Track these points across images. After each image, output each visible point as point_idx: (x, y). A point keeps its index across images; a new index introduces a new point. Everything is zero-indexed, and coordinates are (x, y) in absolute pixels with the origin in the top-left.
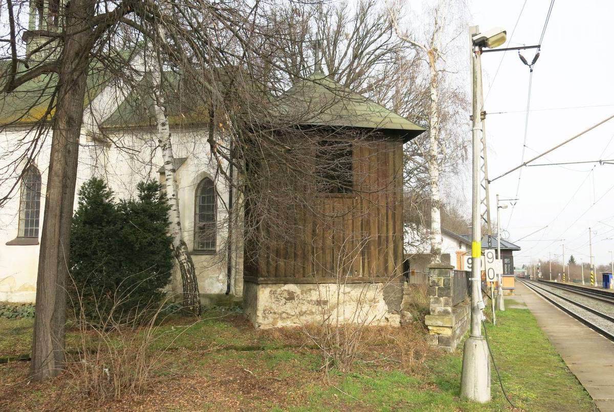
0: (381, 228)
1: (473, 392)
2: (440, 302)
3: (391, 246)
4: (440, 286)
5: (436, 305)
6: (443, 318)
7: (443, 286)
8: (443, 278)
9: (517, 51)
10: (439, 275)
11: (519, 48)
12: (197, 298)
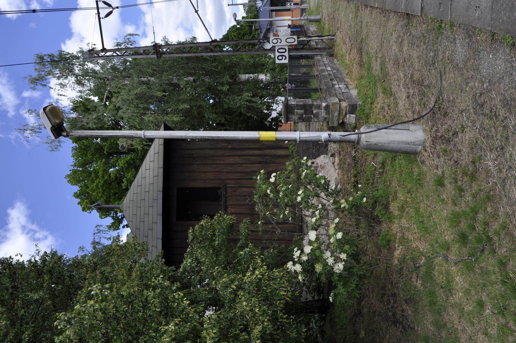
1: (414, 146)
2: (317, 113)
3: (267, 152)
5: (320, 116)
6: (332, 111)
9: (101, 19)
10: (293, 113)
11: (99, 18)
12: (313, 304)
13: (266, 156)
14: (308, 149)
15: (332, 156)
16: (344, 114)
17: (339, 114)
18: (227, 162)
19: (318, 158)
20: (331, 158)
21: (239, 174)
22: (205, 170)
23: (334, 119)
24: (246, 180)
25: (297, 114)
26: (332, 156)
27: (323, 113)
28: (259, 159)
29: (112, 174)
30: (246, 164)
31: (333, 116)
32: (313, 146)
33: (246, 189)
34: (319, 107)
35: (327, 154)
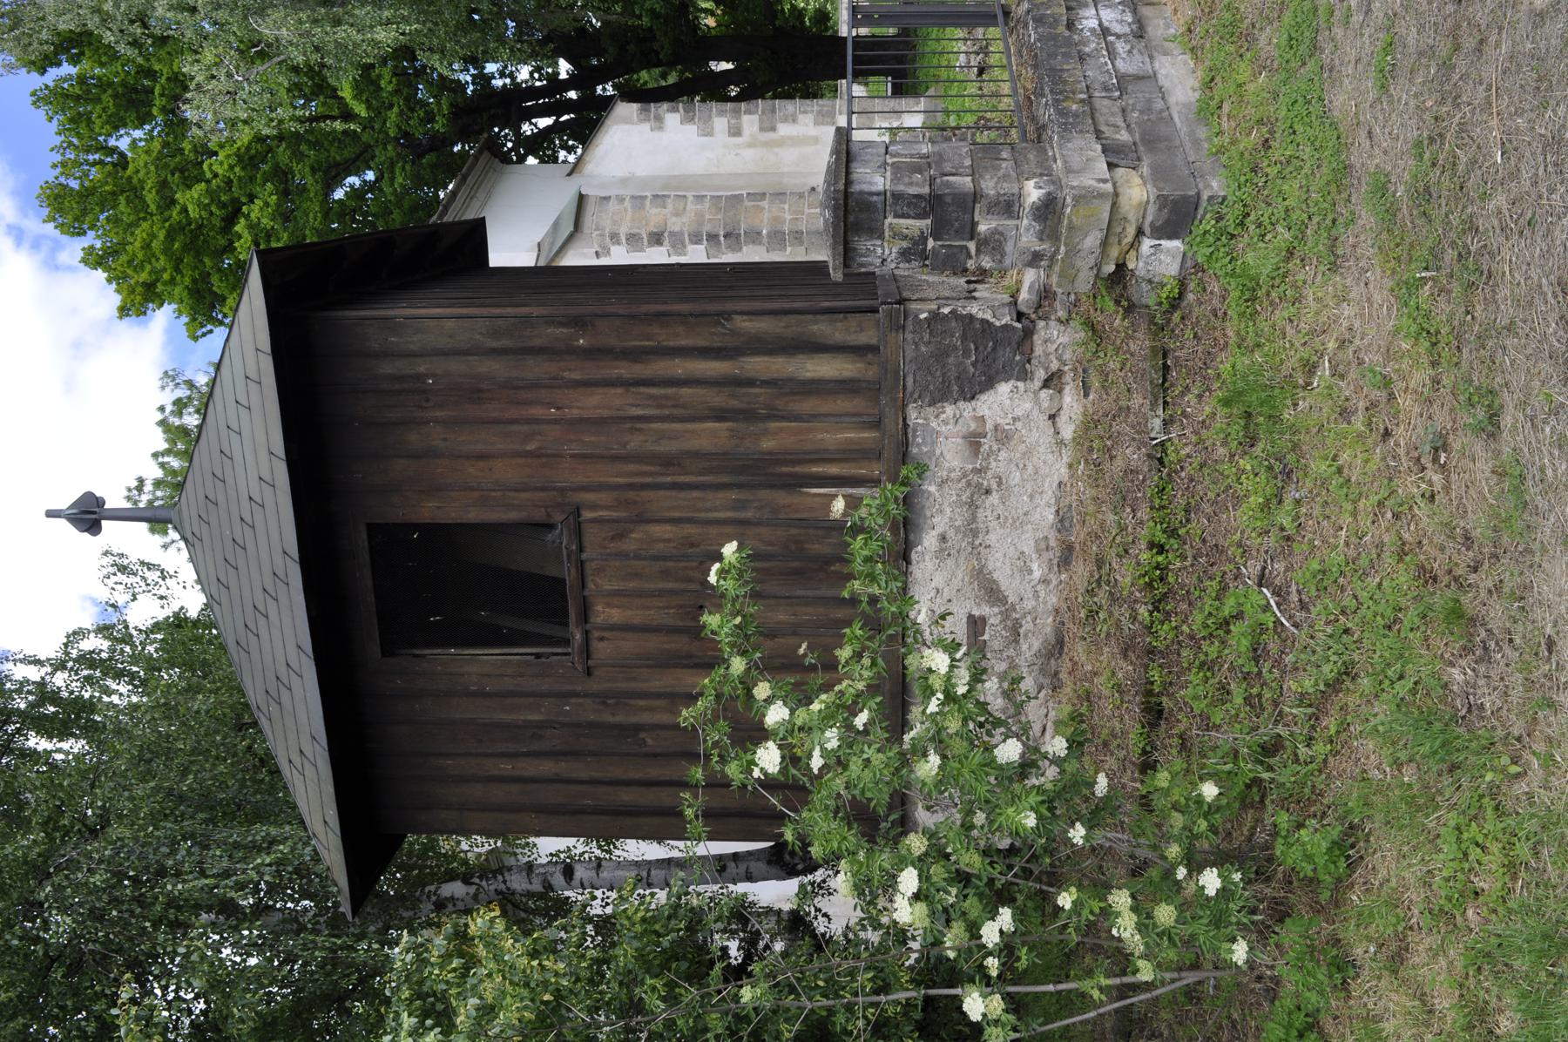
0: (684, 407)
2: (995, 232)
3: (756, 365)
4: (927, 232)
5: (1009, 247)
6: (1071, 228)
7: (929, 221)
8: (889, 220)
13: (751, 382)
14: (941, 355)
15: (1046, 384)
16: (1129, 239)
17: (1105, 244)
18: (576, 412)
19: (983, 397)
20: (1044, 394)
21: (632, 467)
22: (480, 447)
23: (1078, 263)
24: (662, 493)
25: (897, 235)
26: (1046, 384)
27: (1025, 234)
28: (717, 398)
29: (190, 208)
30: (662, 419)
31: (1073, 251)
32: (964, 338)
33: (668, 527)
34: (1008, 206)
35: (1024, 376)
